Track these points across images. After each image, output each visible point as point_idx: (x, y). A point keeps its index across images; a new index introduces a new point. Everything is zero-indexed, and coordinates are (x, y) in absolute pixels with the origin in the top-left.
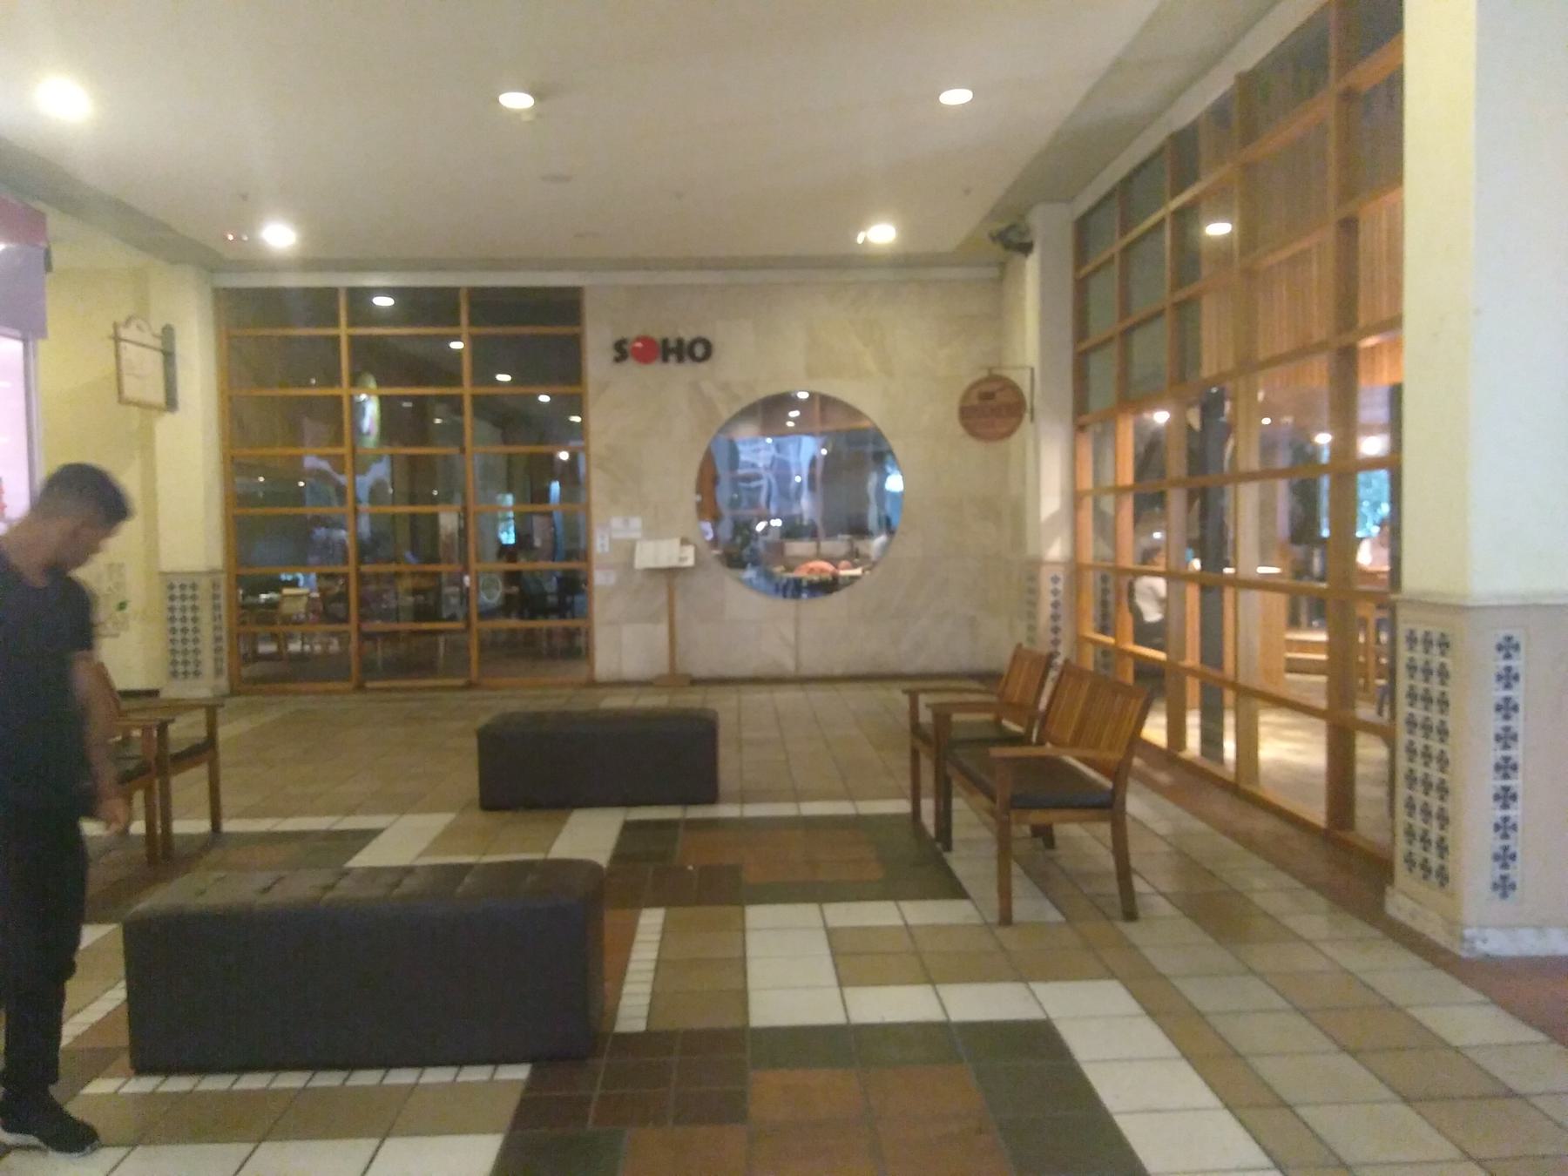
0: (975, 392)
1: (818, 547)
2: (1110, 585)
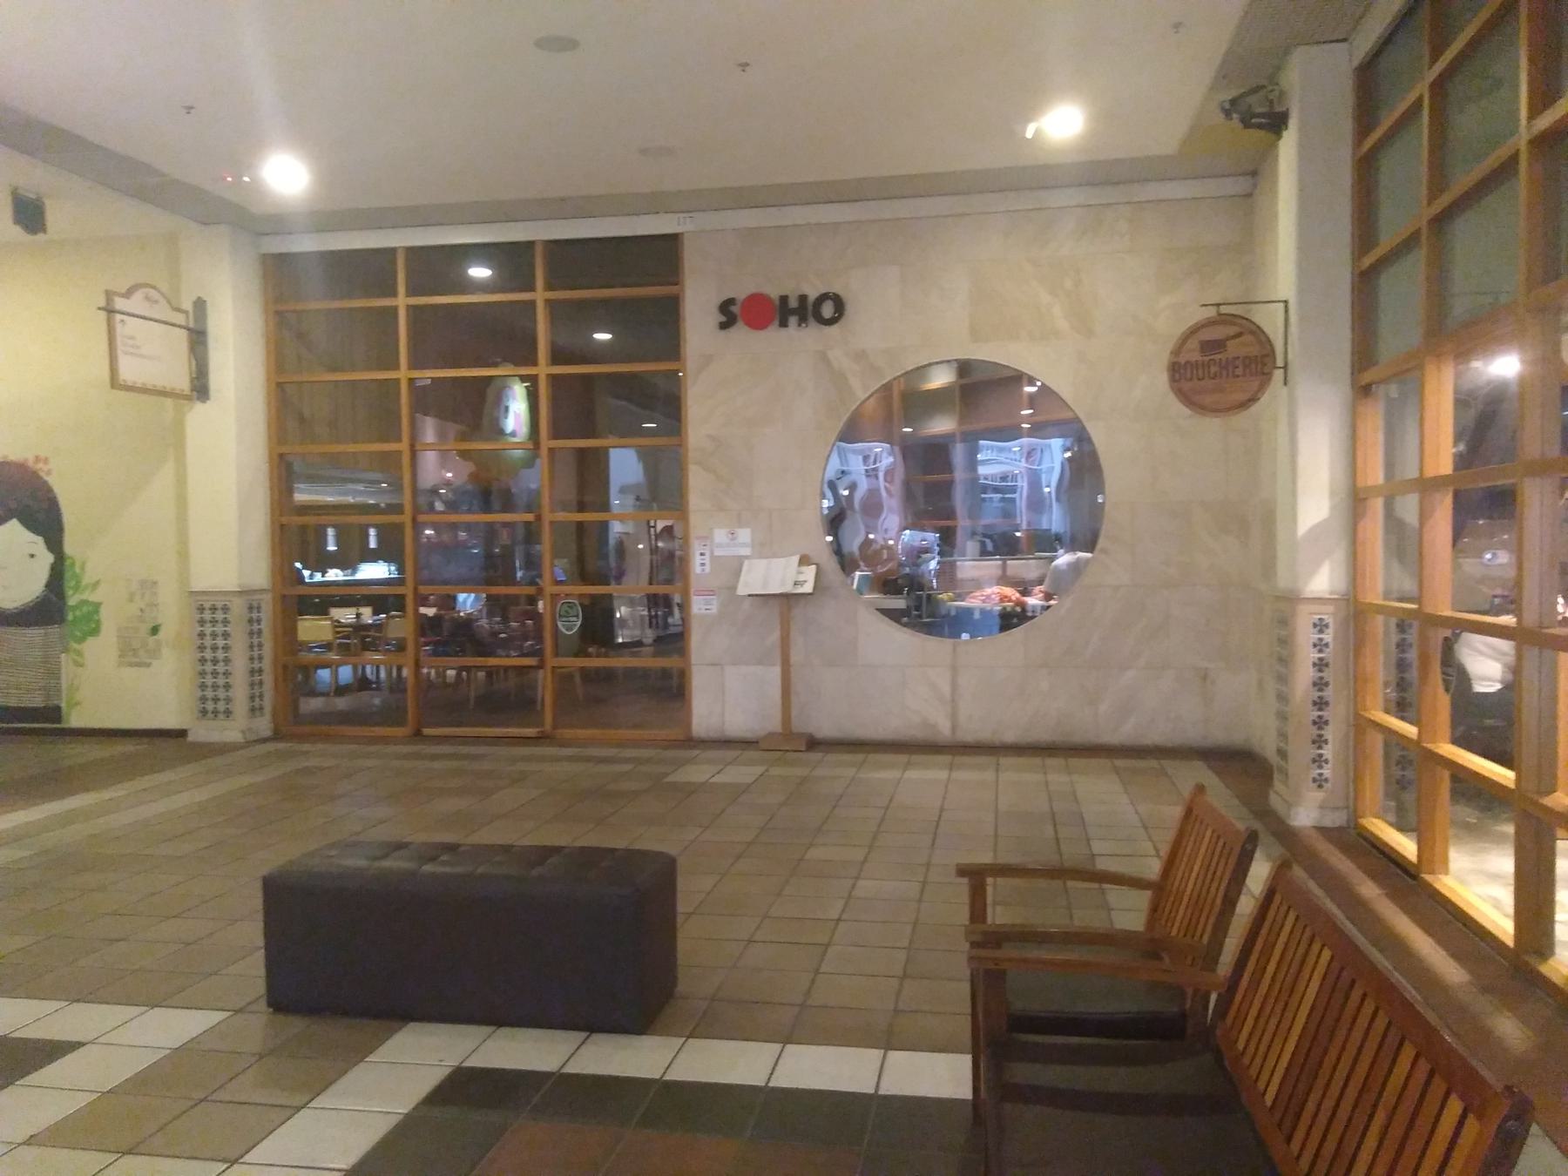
0: (1193, 344)
1: (1004, 567)
2: (1412, 636)
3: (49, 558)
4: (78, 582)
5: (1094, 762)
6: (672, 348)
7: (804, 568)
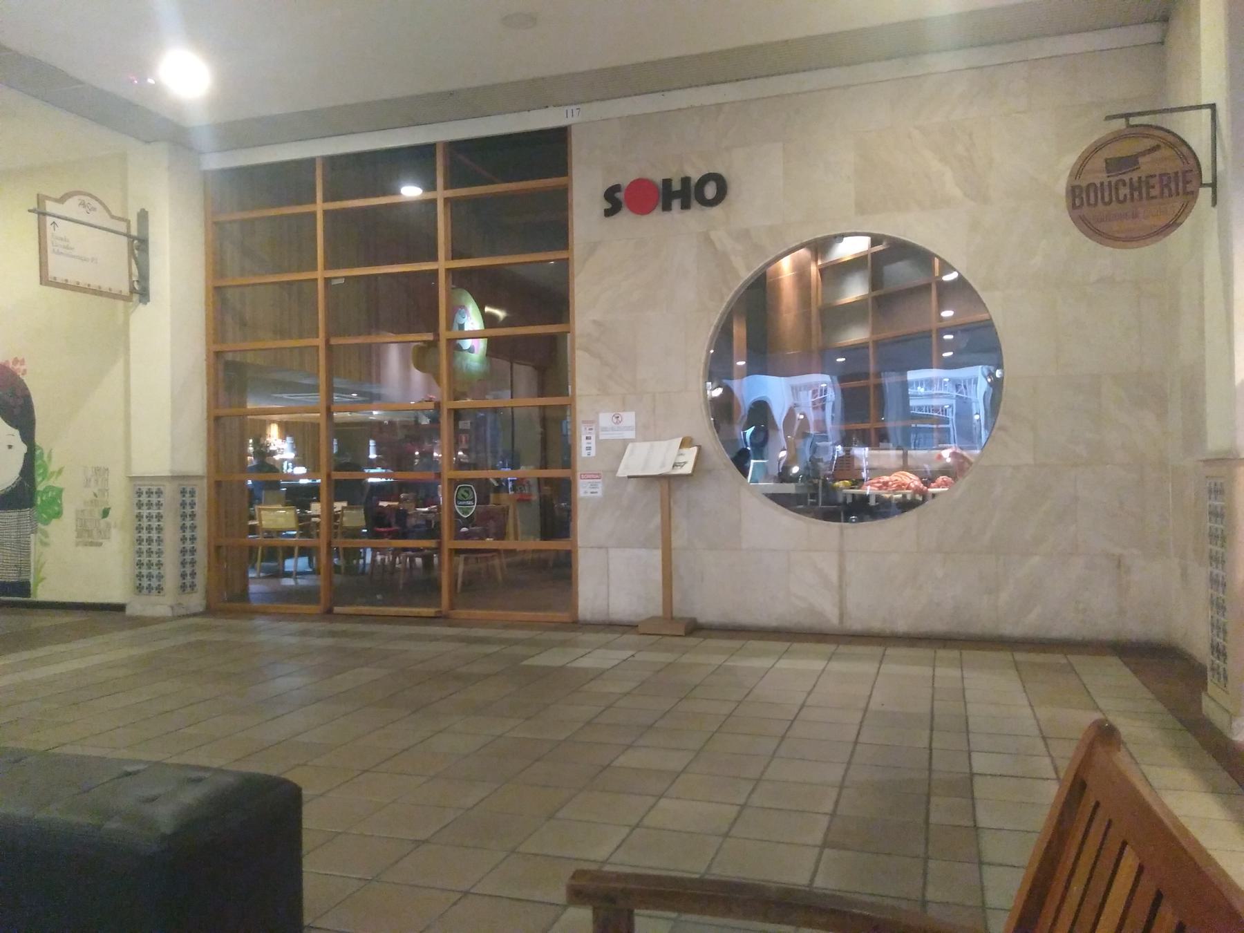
0: (1099, 162)
1: (905, 456)
3: (23, 448)
4: (46, 470)
5: (991, 655)
6: (557, 232)
7: (685, 450)
